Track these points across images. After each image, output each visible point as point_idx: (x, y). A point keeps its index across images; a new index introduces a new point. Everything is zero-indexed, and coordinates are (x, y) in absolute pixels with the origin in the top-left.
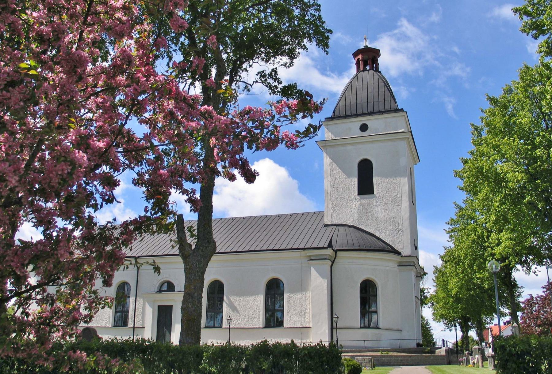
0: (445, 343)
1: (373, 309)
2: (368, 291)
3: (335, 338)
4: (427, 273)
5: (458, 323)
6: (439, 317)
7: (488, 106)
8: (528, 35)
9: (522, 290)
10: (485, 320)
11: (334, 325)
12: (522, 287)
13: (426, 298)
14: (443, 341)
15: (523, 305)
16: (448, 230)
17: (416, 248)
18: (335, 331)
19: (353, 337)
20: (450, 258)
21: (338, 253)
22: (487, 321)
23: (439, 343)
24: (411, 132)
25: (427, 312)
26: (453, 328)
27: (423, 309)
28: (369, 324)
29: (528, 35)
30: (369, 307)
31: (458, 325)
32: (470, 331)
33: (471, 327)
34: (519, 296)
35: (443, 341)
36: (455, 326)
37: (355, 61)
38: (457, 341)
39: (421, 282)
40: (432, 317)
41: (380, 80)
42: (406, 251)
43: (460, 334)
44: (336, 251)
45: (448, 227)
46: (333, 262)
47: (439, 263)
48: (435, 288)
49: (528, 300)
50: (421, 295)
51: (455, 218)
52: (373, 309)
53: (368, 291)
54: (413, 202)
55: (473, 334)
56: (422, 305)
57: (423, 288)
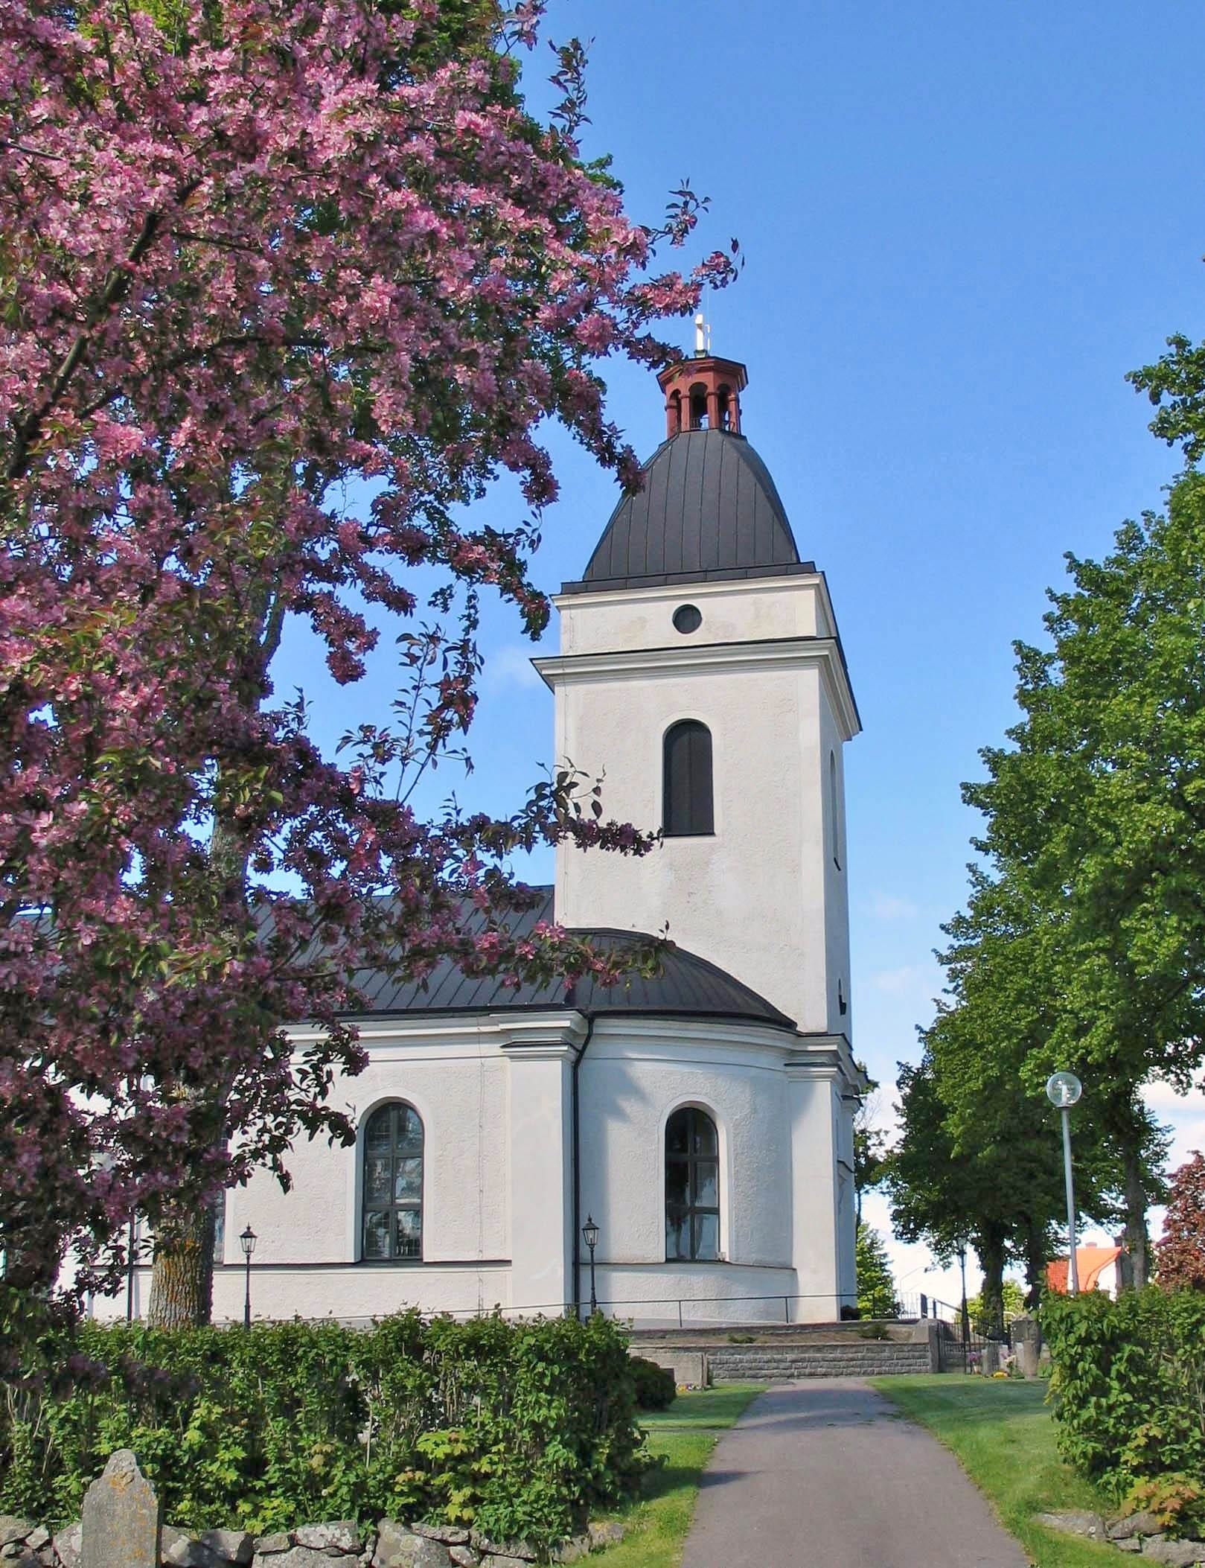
0: (930, 1305)
1: (703, 1203)
2: (689, 1134)
3: (586, 1296)
4: (875, 1085)
5: (973, 1242)
6: (910, 1223)
7: (1067, 585)
8: (1170, 445)
9: (1169, 1137)
10: (1056, 1233)
11: (585, 1252)
12: (1168, 1129)
13: (872, 1162)
14: (924, 1299)
15: (1169, 1184)
16: (946, 952)
17: (844, 1008)
18: (585, 1274)
19: (645, 1299)
20: (947, 1039)
21: (598, 1021)
22: (1062, 1235)
23: (911, 1308)
24: (837, 639)
25: (877, 1208)
26: (955, 1259)
27: (864, 1197)
28: (693, 1252)
29: (1170, 445)
30: (695, 1195)
31: (969, 1249)
32: (1007, 1268)
33: (1010, 1254)
34: (1160, 1156)
35: (924, 1299)
36: (962, 1253)
37: (664, 400)
38: (964, 1301)
39: (858, 1115)
40: (891, 1226)
41: (743, 465)
42: (810, 1013)
43: (976, 1278)
44: (590, 1018)
45: (946, 943)
46: (581, 1053)
47: (916, 1056)
48: (902, 1134)
49: (1188, 1167)
50: (857, 1155)
51: (968, 913)
52: (703, 1203)
53: (689, 1134)
54: (836, 862)
55: (1015, 1274)
56: (859, 1186)
57: (863, 1132)
